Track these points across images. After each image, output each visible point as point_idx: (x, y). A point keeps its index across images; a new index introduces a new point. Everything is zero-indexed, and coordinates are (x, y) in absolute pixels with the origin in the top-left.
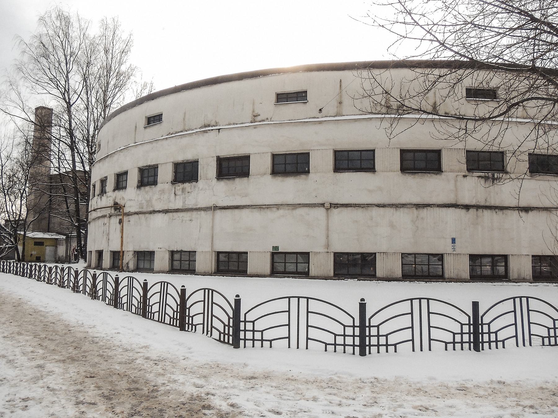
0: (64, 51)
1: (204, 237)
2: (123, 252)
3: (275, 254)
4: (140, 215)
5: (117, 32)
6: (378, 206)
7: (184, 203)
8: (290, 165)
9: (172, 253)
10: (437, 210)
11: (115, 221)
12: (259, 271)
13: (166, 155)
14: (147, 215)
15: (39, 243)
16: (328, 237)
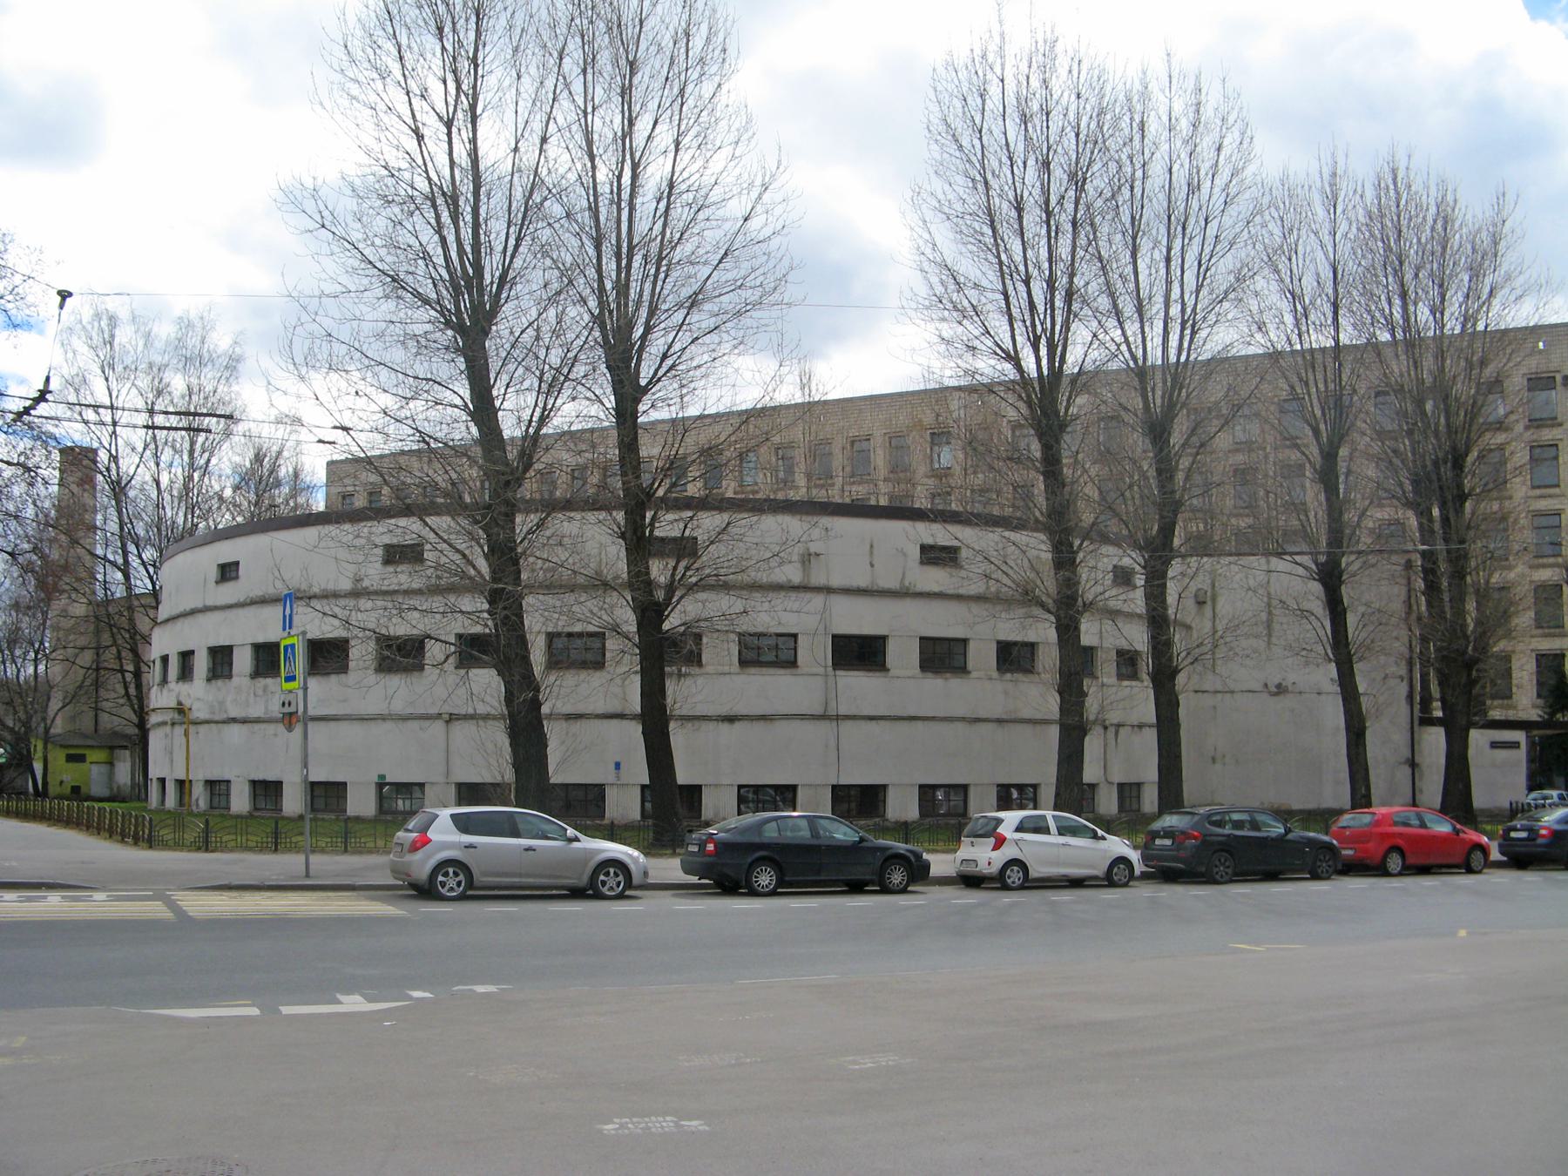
10: (597, 722)
11: (179, 730)
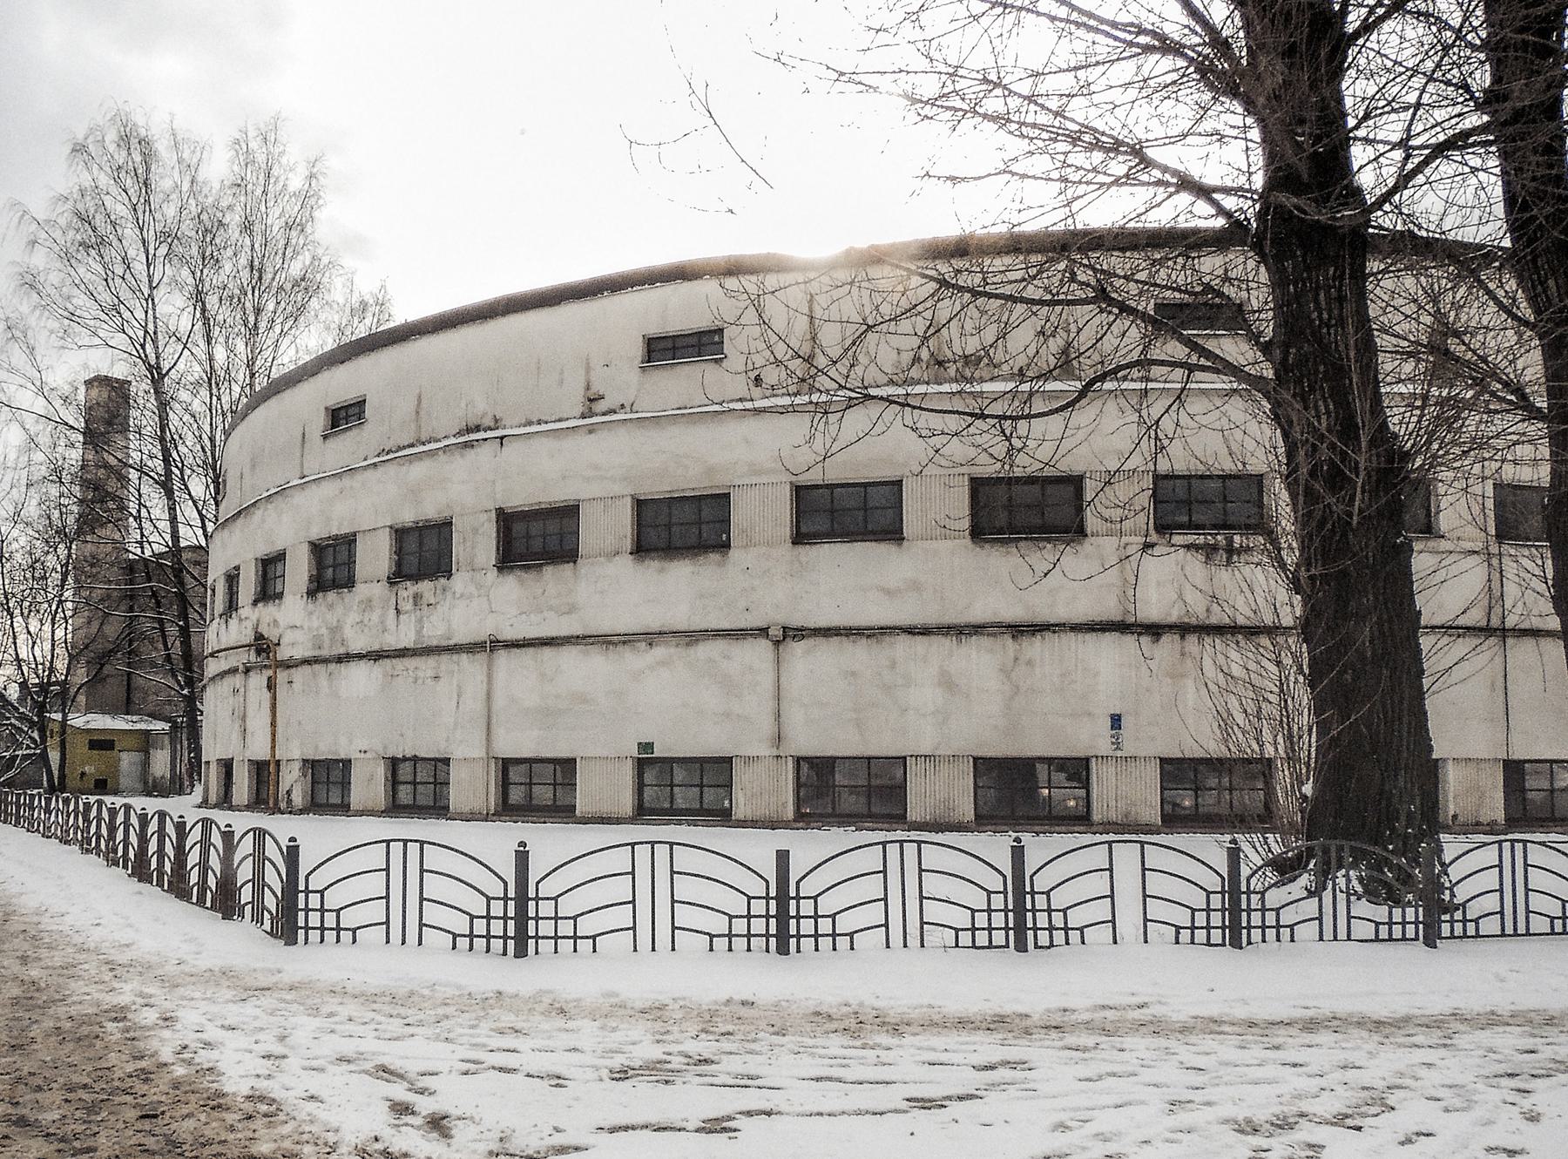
0: (142, 230)
1: (448, 716)
2: (278, 763)
3: (646, 762)
4: (316, 667)
5: (275, 172)
6: (910, 631)
7: (419, 632)
8: (681, 527)
9: (394, 763)
10: (1070, 639)
11: (258, 681)
12: (605, 809)
13: (372, 507)
14: (332, 666)
15: (102, 743)
16: (778, 715)
